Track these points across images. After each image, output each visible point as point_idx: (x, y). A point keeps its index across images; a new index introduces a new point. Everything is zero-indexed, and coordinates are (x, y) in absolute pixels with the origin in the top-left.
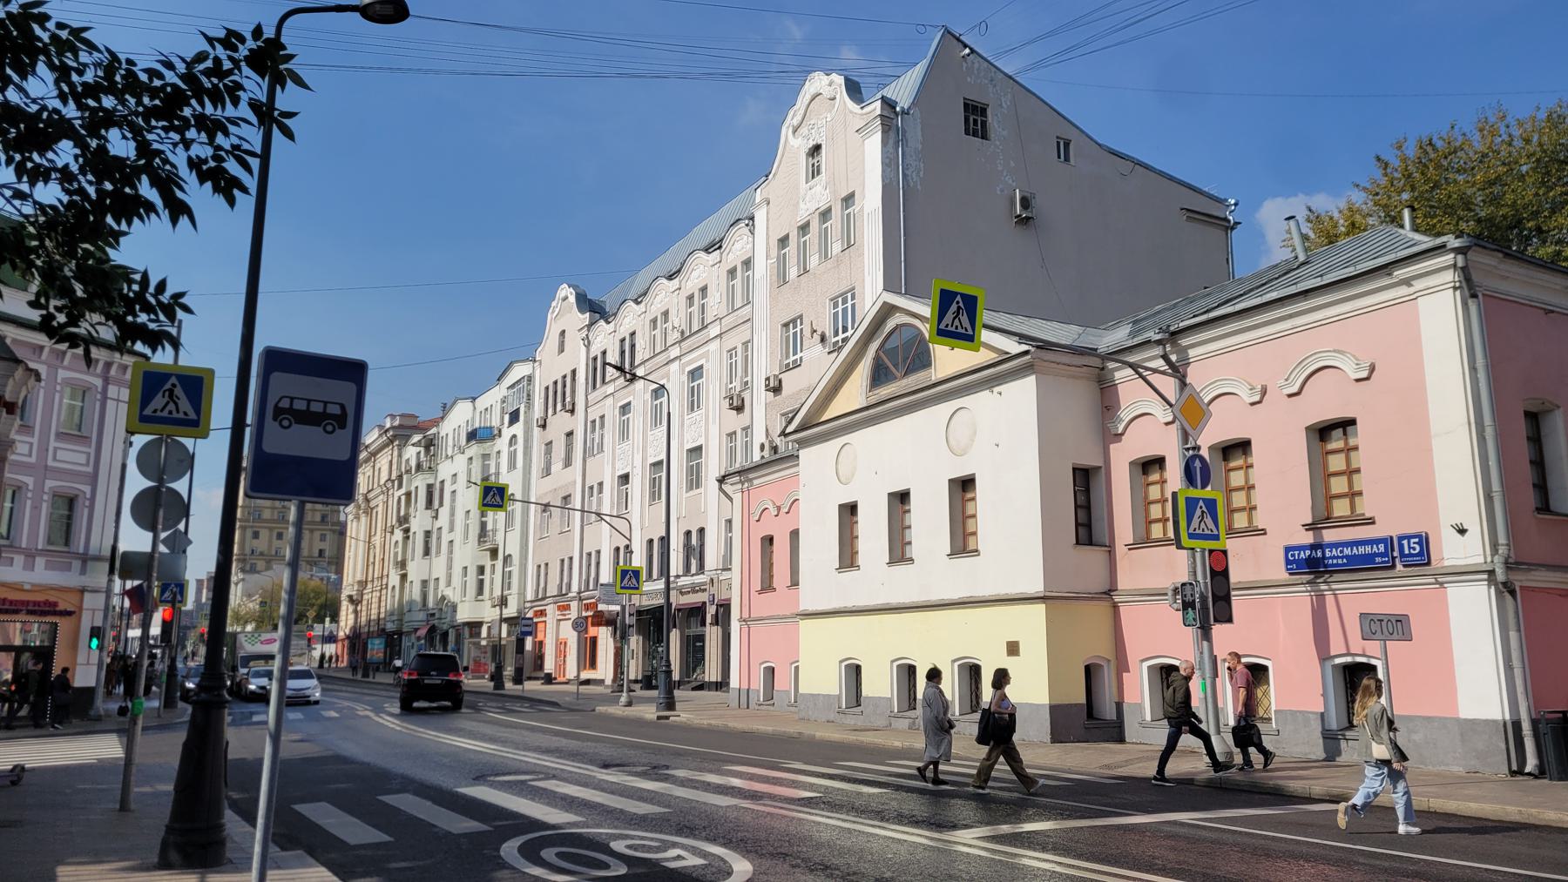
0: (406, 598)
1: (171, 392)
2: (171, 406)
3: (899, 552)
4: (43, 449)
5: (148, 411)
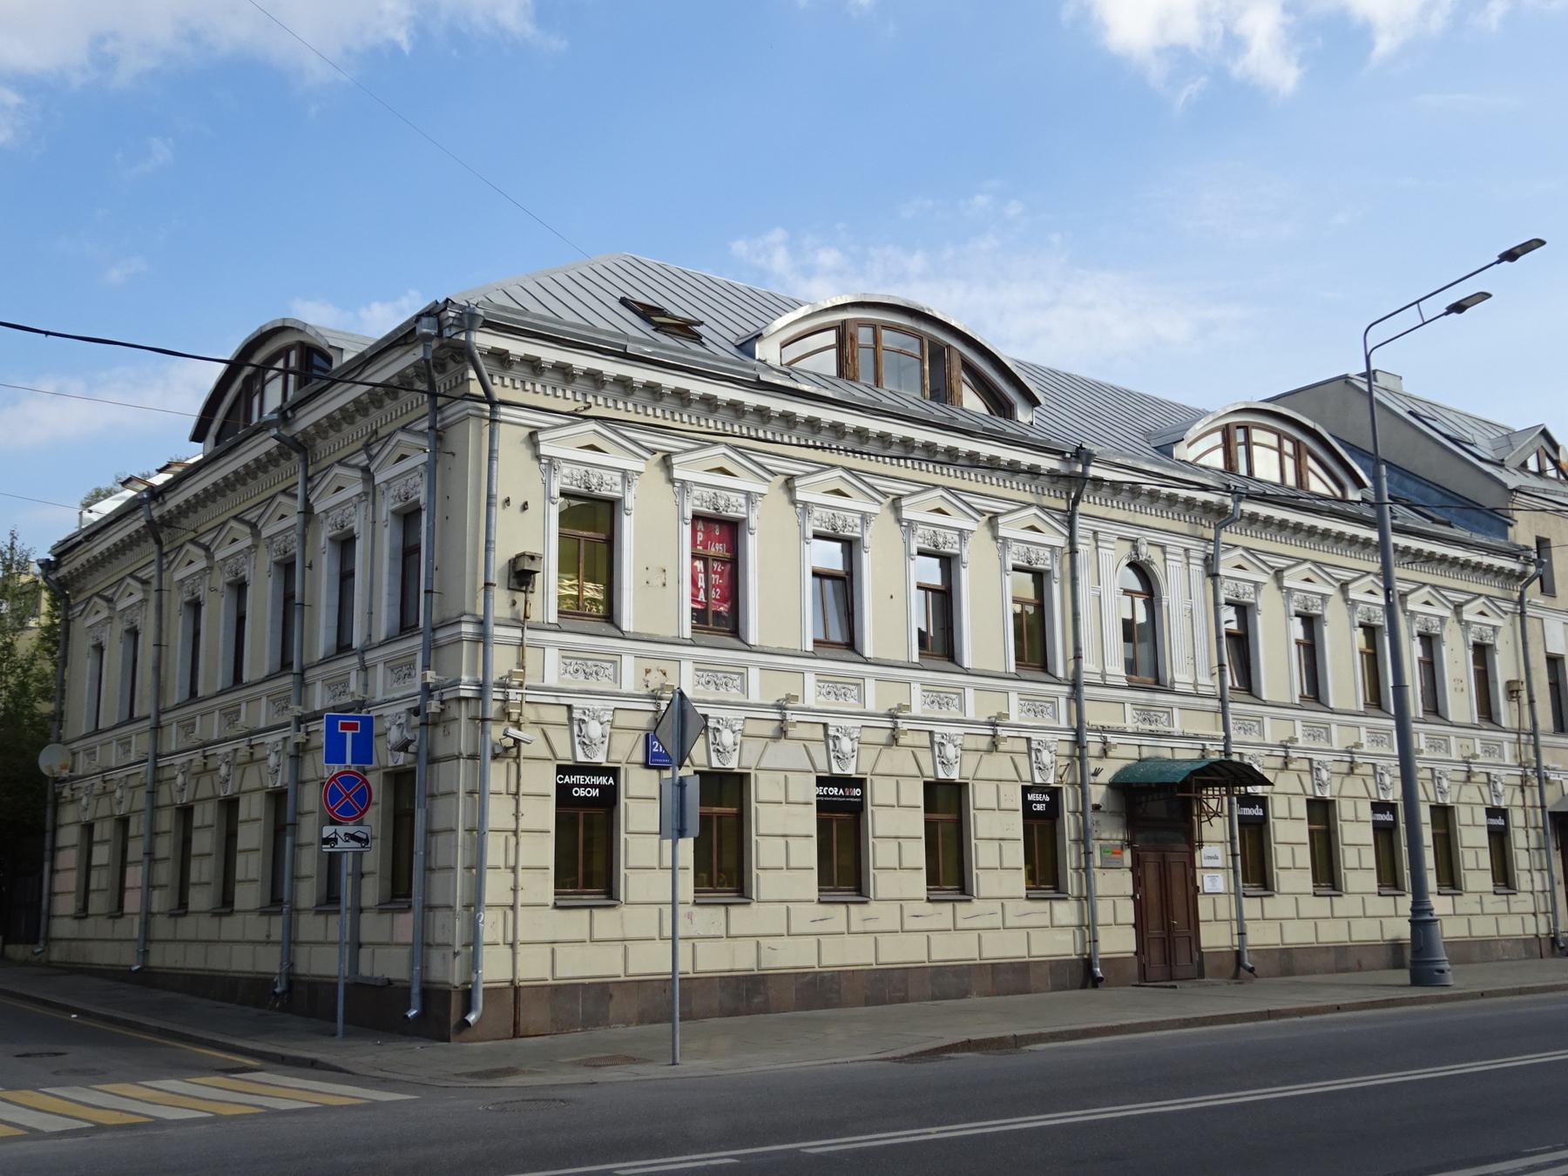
3: (1327, 873)
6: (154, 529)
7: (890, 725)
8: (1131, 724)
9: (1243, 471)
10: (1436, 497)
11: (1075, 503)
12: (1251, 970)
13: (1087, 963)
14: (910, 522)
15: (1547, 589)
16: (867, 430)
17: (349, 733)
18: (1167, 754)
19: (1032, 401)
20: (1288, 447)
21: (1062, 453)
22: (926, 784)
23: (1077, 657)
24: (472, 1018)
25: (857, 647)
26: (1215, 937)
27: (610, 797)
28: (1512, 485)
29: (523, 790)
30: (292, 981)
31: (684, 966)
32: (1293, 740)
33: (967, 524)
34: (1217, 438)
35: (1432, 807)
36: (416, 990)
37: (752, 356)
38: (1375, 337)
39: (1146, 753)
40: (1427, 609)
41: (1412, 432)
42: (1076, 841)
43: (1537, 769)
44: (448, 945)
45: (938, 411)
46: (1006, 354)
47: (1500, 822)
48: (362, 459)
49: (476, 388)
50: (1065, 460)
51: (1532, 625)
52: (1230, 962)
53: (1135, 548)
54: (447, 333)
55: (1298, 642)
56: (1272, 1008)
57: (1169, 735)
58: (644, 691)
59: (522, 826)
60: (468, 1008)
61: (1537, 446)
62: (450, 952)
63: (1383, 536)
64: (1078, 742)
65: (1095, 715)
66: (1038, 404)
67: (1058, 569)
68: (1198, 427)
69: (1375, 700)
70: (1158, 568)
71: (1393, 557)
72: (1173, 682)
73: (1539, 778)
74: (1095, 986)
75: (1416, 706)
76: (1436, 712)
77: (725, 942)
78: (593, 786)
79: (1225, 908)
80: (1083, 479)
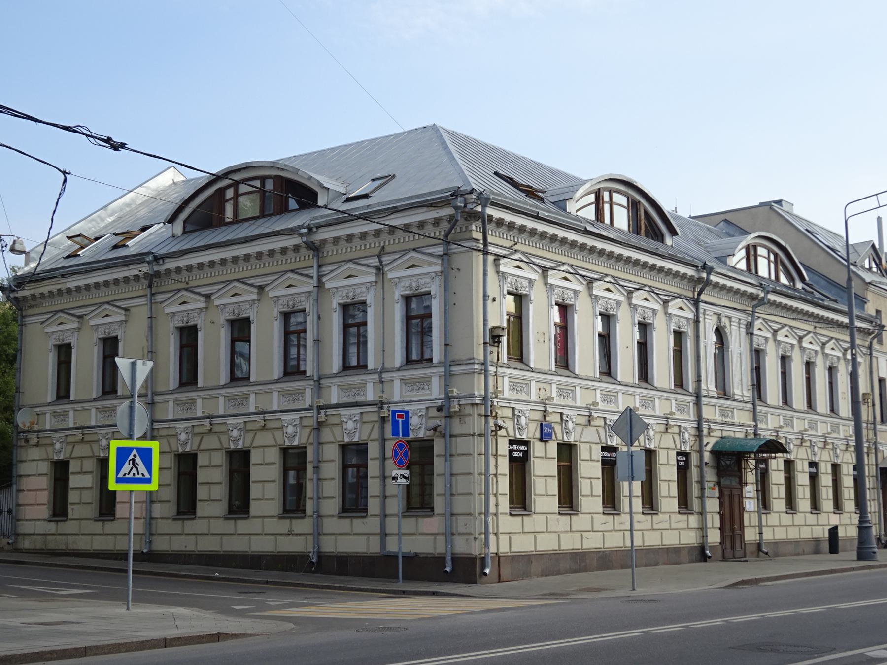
0: (498, 240)
1: (133, 460)
3: (568, 499)
4: (318, 533)
5: (120, 475)
6: (152, 278)
7: (543, 409)
8: (719, 419)
9: (607, 220)
10: (823, 283)
11: (699, 294)
12: (766, 553)
13: (702, 548)
14: (635, 305)
15: (880, 342)
16: (613, 252)
17: (400, 420)
18: (732, 434)
19: (673, 232)
20: (772, 257)
21: (697, 267)
22: (558, 444)
23: (699, 381)
24: (487, 571)
25: (612, 374)
26: (750, 535)
27: (526, 454)
28: (868, 280)
29: (499, 453)
30: (320, 555)
31: (638, 543)
32: (595, 404)
33: (534, 276)
34: (592, 198)
35: (785, 461)
36: (449, 558)
37: (565, 210)
38: (851, 210)
39: (725, 434)
40: (645, 304)
41: (810, 243)
42: (697, 482)
43: (875, 443)
44: (470, 534)
45: (653, 245)
46: (667, 208)
47: (814, 470)
48: (375, 261)
49: (479, 236)
50: (698, 271)
51: (874, 360)
52: (755, 548)
53: (720, 319)
54: (470, 206)
55: (556, 325)
56: (745, 578)
57: (732, 424)
58: (539, 400)
59: (499, 472)
60: (483, 566)
61: (869, 253)
62: (472, 537)
63: (851, 321)
64: (699, 429)
65: (707, 413)
66: (677, 234)
67: (689, 330)
68: (581, 191)
69: (680, 382)
70: (727, 330)
71: (856, 333)
72: (734, 394)
73: (876, 449)
74: (705, 561)
75: (709, 385)
76: (566, 367)
77: (570, 534)
78: (520, 451)
79: (754, 520)
80: (708, 283)
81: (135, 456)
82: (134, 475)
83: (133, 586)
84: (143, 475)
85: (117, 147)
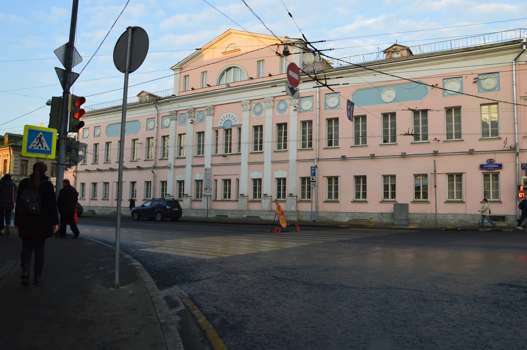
1: (40, 138)
2: (40, 145)
5: (30, 147)
28: (351, 125)
81: (41, 136)
82: (40, 148)
83: (422, 125)
84: (46, 148)
85: (289, 13)
